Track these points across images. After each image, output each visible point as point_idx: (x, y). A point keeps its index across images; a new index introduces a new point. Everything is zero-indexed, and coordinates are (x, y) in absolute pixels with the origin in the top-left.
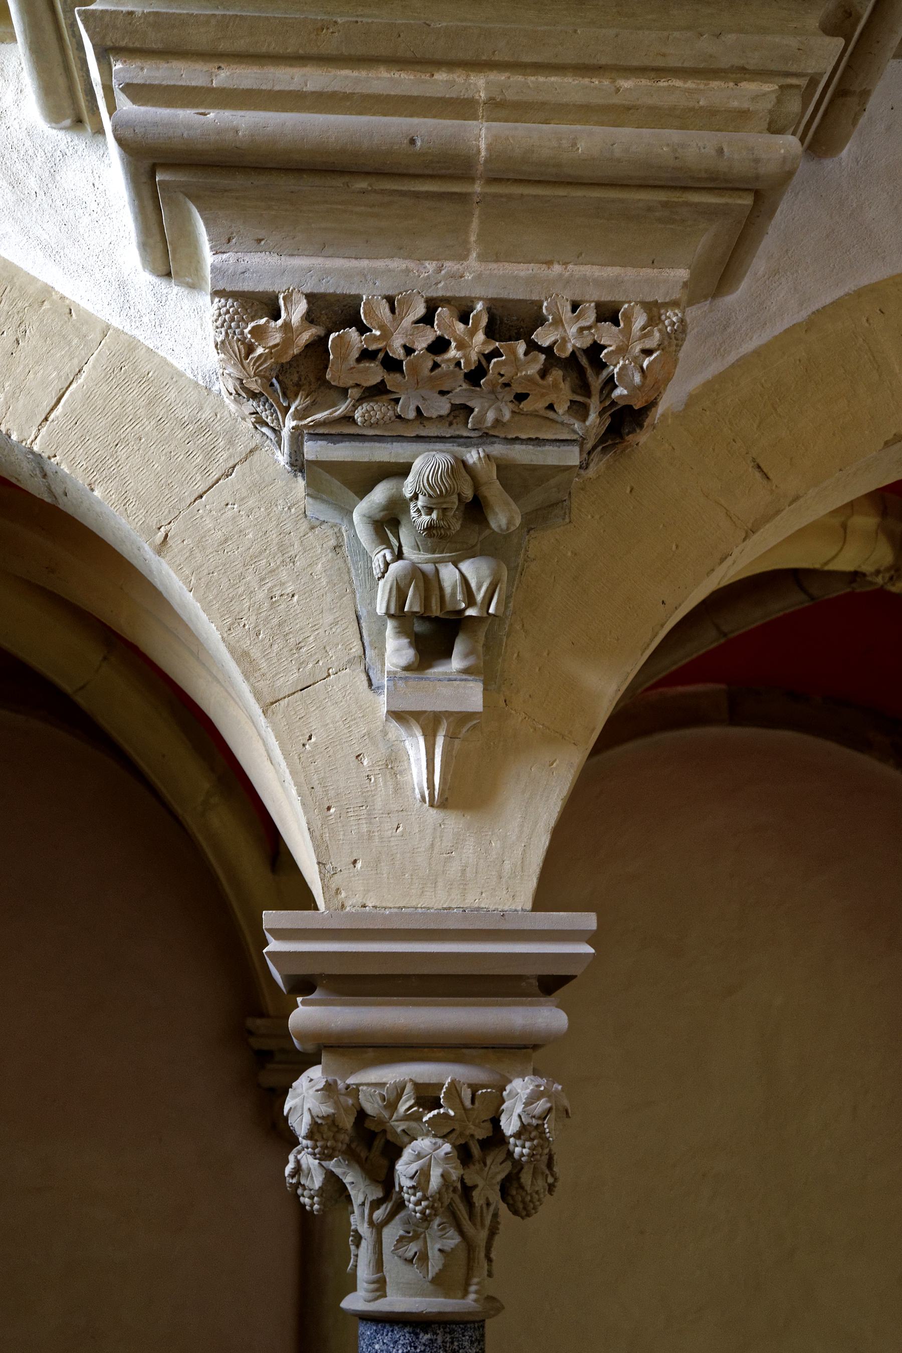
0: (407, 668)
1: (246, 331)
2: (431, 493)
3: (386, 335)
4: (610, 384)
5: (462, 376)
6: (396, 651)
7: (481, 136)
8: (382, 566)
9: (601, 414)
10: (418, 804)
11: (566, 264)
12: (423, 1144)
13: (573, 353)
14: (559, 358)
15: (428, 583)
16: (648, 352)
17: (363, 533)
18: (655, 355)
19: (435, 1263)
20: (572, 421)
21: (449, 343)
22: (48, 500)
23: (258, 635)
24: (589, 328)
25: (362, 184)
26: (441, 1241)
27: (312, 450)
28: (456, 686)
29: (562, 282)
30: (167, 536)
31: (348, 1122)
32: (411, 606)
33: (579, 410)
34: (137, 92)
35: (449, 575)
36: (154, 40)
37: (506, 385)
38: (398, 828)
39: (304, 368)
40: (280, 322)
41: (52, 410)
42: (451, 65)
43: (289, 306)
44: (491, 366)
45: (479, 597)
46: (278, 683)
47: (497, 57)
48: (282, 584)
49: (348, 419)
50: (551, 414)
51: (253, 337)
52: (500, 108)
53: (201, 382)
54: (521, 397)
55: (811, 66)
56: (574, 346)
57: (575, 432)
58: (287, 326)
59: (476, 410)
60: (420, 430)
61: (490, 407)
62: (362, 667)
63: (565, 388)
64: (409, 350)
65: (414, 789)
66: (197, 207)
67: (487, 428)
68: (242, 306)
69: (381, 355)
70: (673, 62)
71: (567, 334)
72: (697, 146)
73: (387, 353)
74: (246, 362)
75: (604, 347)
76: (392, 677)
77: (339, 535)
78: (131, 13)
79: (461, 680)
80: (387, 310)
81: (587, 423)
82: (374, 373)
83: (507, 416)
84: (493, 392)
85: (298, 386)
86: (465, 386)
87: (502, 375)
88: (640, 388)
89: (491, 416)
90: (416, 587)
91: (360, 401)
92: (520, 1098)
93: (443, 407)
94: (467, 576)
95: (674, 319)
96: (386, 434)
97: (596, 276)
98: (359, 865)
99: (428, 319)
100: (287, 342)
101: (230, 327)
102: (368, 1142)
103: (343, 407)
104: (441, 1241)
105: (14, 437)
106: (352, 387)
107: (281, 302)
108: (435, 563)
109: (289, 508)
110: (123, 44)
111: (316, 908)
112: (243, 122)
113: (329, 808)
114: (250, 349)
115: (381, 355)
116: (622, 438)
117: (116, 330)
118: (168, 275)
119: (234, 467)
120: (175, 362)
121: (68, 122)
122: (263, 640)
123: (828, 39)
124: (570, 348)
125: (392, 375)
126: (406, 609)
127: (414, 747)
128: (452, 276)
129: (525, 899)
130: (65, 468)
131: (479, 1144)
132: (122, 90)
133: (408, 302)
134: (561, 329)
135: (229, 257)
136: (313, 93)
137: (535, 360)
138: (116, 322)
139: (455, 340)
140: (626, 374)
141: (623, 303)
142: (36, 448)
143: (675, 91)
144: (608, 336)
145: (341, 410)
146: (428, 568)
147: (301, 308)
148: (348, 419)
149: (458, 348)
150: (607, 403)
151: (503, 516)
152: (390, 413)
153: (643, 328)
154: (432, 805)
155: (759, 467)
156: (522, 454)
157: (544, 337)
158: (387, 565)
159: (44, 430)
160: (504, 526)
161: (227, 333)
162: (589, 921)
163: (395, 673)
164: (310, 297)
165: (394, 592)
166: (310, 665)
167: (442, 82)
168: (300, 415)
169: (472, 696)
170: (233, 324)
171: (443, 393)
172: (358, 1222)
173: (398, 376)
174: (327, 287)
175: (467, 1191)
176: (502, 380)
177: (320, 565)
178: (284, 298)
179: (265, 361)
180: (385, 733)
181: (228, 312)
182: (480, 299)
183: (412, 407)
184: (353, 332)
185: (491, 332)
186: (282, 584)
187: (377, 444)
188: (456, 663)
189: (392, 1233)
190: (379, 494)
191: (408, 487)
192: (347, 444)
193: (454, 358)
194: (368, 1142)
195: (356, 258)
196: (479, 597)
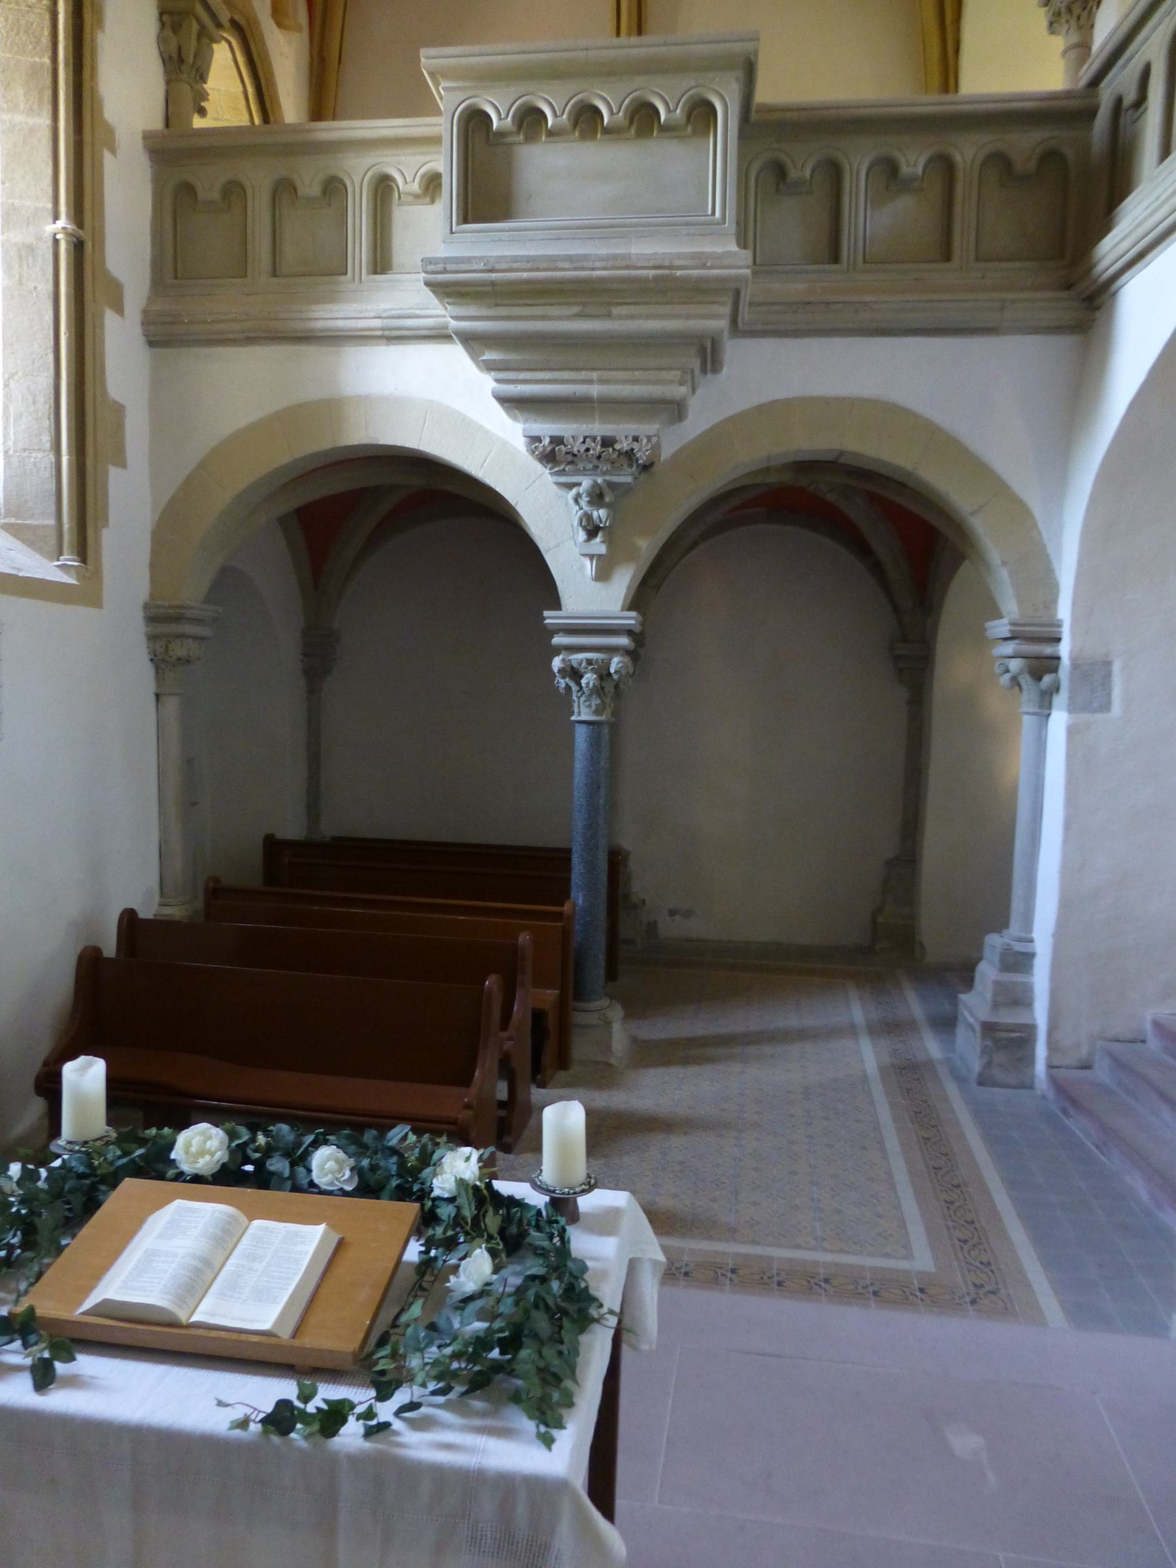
6: (582, 535)
12: (588, 675)
15: (588, 517)
17: (571, 502)
19: (594, 707)
26: (596, 701)
29: (623, 430)
31: (568, 669)
33: (631, 466)
35: (595, 514)
42: (587, 369)
52: (601, 381)
60: (584, 472)
71: (624, 445)
72: (655, 391)
82: (570, 458)
92: (616, 663)
93: (590, 466)
94: (600, 514)
99: (584, 442)
102: (575, 674)
104: (596, 701)
127: (587, 562)
129: (619, 607)
131: (604, 675)
140: (642, 457)
143: (652, 375)
144: (636, 446)
145: (562, 467)
148: (564, 470)
156: (615, 479)
157: (617, 447)
162: (547, 621)
167: (583, 375)
169: (602, 549)
172: (575, 698)
174: (555, 433)
175: (603, 688)
189: (582, 699)
191: (581, 490)
194: (575, 674)
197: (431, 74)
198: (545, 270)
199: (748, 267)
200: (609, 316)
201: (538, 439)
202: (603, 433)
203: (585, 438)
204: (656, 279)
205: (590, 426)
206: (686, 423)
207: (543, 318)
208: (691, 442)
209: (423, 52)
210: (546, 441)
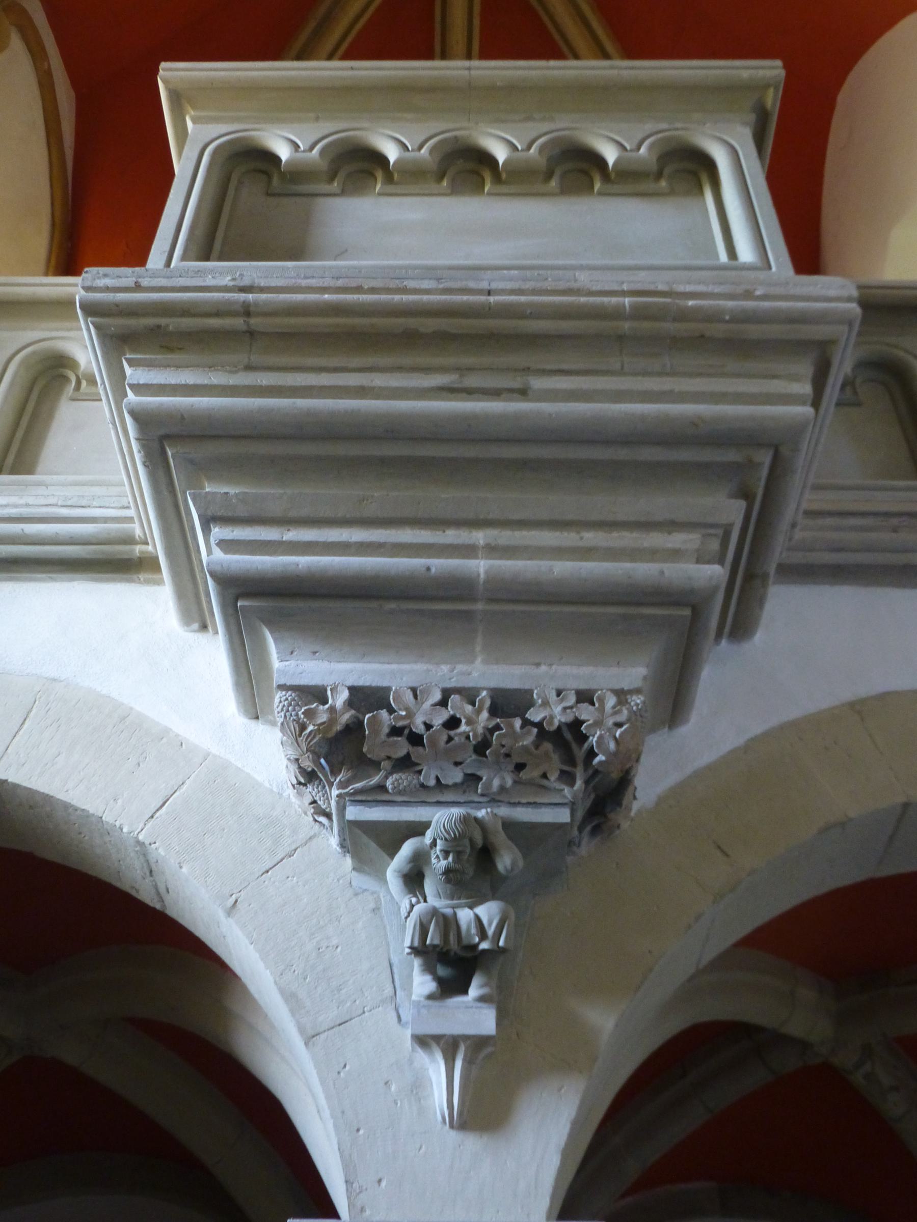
0: (431, 997)
1: (300, 713)
2: (447, 836)
3: (410, 715)
4: (591, 754)
5: (471, 748)
6: (423, 984)
7: (480, 567)
8: (408, 907)
9: (587, 782)
10: (439, 1125)
11: (551, 665)
13: (559, 728)
14: (549, 732)
15: (448, 923)
16: (619, 725)
18: (625, 727)
20: (563, 786)
21: (459, 721)
22: (158, 906)
23: (305, 979)
24: (571, 707)
25: (392, 605)
27: (353, 813)
28: (473, 1014)
30: (236, 901)
32: (432, 939)
33: (567, 777)
34: (227, 545)
35: (465, 916)
36: (242, 511)
37: (508, 755)
38: (420, 1148)
39: (346, 748)
40: (327, 706)
41: (158, 810)
43: (334, 695)
44: (494, 738)
45: (491, 931)
46: (320, 1019)
47: (491, 516)
48: (328, 938)
49: (381, 788)
50: (545, 782)
51: (305, 717)
52: (492, 550)
53: (275, 790)
54: (520, 767)
55: (724, 519)
56: (560, 721)
57: (565, 797)
58: (332, 709)
59: (484, 778)
61: (495, 776)
62: (393, 1006)
63: (555, 757)
64: (428, 726)
65: (436, 1113)
66: (269, 630)
67: (494, 793)
68: (298, 696)
69: (406, 732)
70: (621, 517)
71: (557, 714)
73: (411, 730)
74: (300, 739)
75: (583, 722)
76: (417, 1004)
77: (378, 901)
78: (227, 493)
79: (477, 1008)
80: (411, 696)
81: (575, 788)
82: (402, 747)
83: (509, 782)
84: (497, 763)
85: (342, 764)
86: (474, 757)
87: (503, 746)
88: (615, 754)
89: (496, 783)
90: (437, 922)
91: (391, 773)
93: (455, 776)
95: (638, 701)
96: (412, 800)
97: (575, 673)
98: (384, 1184)
99: (443, 703)
100: (332, 721)
101: (288, 711)
103: (377, 778)
105: (125, 830)
106: (384, 760)
107: (329, 693)
108: (453, 908)
109: (338, 880)
110: (219, 514)
111: (335, 1215)
112: (303, 562)
113: (358, 1130)
114: (303, 727)
115: (406, 732)
116: (605, 816)
117: (215, 756)
118: (257, 718)
119: (295, 850)
120: (256, 776)
121: (196, 626)
122: (309, 983)
123: (733, 501)
124: (556, 723)
125: (415, 748)
126: (428, 942)
128: (462, 674)
130: (162, 852)
132: (218, 544)
133: (427, 692)
134: (548, 709)
135: (291, 664)
136: (356, 543)
137: (529, 733)
138: (214, 750)
139: (465, 718)
141: (596, 690)
142: (141, 837)
144: (586, 713)
145: (375, 780)
146: (448, 911)
147: (344, 695)
148: (381, 788)
149: (468, 724)
150: (590, 772)
151: (506, 860)
152: (415, 781)
153: (614, 707)
154: (452, 1126)
155: (719, 847)
157: (535, 715)
158: (412, 906)
159: (149, 825)
160: (509, 867)
161: (285, 716)
163: (419, 1002)
164: (352, 689)
165: (418, 928)
166: (348, 1004)
167: (451, 536)
168: (342, 785)
169: (485, 1022)
170: (290, 708)
171: (457, 764)
173: (420, 749)
176: (503, 751)
177: (361, 923)
178: (331, 690)
179: (314, 737)
180: (411, 1062)
181: (287, 699)
182: (517, 920)
183: (433, 776)
184: (384, 713)
185: (494, 711)
186: (328, 938)
187: (405, 808)
188: (474, 991)
190: (407, 848)
192: (381, 808)
193: (464, 732)
195: (388, 663)
196: (491, 931)
197: (176, 97)
198: (373, 290)
199: (849, 299)
200: (523, 393)
201: (318, 694)
202: (493, 684)
203: (447, 694)
204: (635, 307)
205: (460, 667)
206: (688, 729)
207: (361, 392)
208: (698, 775)
209: (171, 74)
210: (340, 699)
